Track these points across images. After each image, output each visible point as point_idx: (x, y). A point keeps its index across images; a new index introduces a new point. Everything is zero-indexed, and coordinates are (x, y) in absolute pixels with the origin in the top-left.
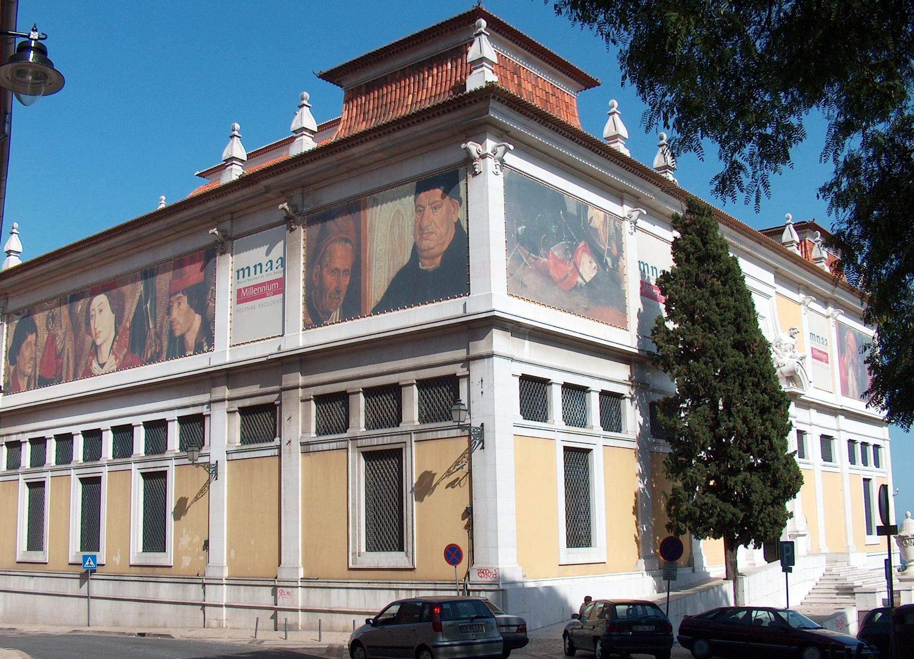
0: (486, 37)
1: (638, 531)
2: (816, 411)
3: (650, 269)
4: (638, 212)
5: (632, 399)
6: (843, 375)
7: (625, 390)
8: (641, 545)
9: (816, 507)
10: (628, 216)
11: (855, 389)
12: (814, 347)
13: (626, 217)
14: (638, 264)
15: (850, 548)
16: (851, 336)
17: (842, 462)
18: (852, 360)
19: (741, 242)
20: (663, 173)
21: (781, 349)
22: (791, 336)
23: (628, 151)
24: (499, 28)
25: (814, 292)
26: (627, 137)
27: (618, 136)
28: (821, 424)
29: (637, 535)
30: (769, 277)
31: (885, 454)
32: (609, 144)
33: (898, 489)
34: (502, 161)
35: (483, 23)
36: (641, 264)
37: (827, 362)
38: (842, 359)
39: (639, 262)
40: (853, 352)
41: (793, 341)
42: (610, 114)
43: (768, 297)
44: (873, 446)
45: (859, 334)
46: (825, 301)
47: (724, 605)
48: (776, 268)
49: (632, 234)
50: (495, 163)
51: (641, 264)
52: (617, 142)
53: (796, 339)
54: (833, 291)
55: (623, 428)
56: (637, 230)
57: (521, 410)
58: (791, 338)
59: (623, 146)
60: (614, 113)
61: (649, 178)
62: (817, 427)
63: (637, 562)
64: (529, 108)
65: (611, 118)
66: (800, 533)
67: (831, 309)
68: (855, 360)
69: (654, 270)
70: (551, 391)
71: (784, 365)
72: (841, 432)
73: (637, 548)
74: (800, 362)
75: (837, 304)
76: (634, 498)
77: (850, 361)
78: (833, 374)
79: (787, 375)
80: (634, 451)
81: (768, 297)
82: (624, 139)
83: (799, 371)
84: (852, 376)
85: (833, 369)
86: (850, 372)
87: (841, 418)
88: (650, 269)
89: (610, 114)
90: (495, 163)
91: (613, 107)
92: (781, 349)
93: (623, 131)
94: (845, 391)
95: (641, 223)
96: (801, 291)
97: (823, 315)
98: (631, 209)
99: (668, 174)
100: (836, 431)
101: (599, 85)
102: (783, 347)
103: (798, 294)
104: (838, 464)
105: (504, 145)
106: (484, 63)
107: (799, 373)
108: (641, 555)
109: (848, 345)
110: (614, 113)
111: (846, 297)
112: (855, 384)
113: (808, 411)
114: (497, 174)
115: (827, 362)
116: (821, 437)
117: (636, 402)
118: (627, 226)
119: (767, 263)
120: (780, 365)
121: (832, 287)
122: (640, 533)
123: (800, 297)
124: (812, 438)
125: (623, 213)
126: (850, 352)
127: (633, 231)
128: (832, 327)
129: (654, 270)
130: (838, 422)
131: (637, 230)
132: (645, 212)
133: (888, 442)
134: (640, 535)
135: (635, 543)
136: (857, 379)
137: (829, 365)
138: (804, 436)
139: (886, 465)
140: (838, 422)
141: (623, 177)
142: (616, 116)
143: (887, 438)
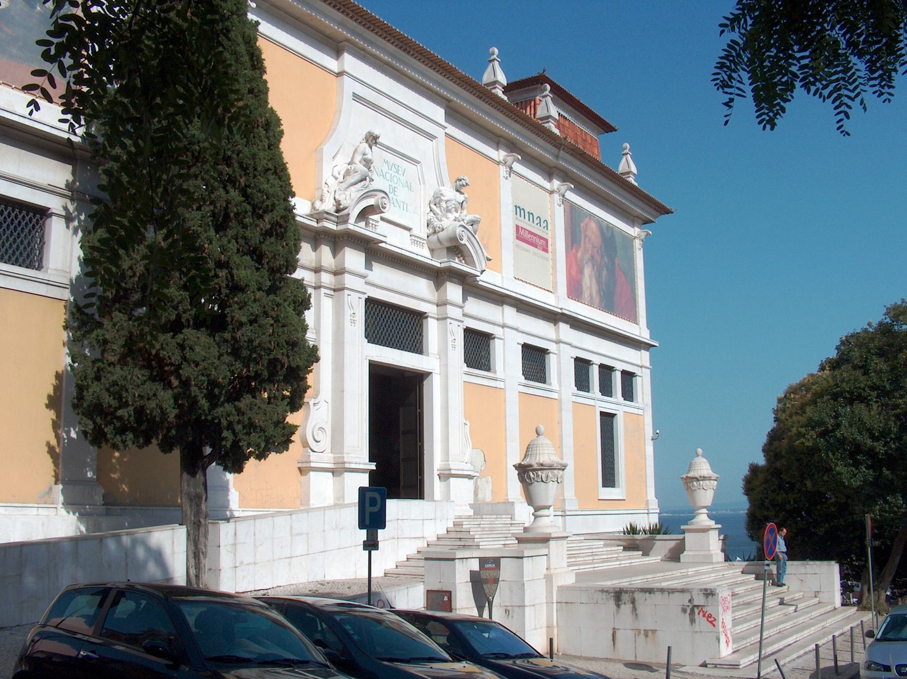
0: (498, 63)
1: (57, 437)
2: (515, 309)
3: (527, 215)
4: (566, 186)
5: (68, 219)
6: (574, 273)
7: (55, 204)
8: (60, 461)
9: (506, 441)
10: (557, 189)
11: (594, 295)
12: (521, 224)
13: (502, 161)
14: (515, 208)
15: (567, 502)
16: (593, 225)
17: (560, 386)
18: (593, 257)
19: (371, 43)
20: (546, 123)
21: (440, 207)
22: (457, 191)
23: (558, 131)
24: (561, 95)
25: (524, 152)
26: (636, 173)
27: (549, 117)
28: (574, 343)
29: (54, 442)
30: (439, 113)
31: (643, 386)
32: (544, 123)
33: (658, 431)
34: (511, 168)
35: (548, 87)
36: (518, 209)
37: (545, 250)
38: (574, 251)
39: (516, 206)
40: (594, 247)
41: (461, 198)
42: (624, 155)
43: (431, 137)
44: (622, 372)
45: (608, 227)
46: (549, 172)
47: (152, 573)
48: (449, 101)
49: (506, 179)
50: (505, 170)
51: (518, 209)
52: (548, 122)
53: (466, 195)
54: (557, 157)
55: (491, 367)
56: (512, 175)
57: (465, 359)
58: (458, 193)
59: (553, 126)
60: (627, 154)
61: (521, 121)
62: (515, 332)
63: (51, 489)
64: (424, 54)
65: (491, 65)
66: (453, 472)
67: (556, 183)
68: (598, 258)
69: (531, 216)
70: (51, 225)
71: (443, 230)
72: (561, 344)
73: (52, 466)
74: (470, 228)
75: (566, 177)
76: (54, 381)
77: (587, 256)
78: (554, 267)
79: (448, 245)
80: (63, 303)
81: (431, 137)
82: (634, 174)
83: (465, 238)
84: (590, 276)
85: (554, 260)
86: (588, 271)
87: (564, 327)
88: (527, 215)
89: (624, 155)
90: (505, 170)
91: (626, 149)
92: (440, 207)
93: (634, 169)
94: (575, 292)
95: (517, 167)
96: (500, 146)
97: (330, 71)
98: (506, 154)
99: (550, 124)
100: (640, 368)
101: (616, 130)
102: (443, 204)
103: (498, 150)
104: (499, 374)
105: (514, 155)
106: (497, 85)
107: (464, 241)
108: (60, 477)
109: (586, 237)
110: (627, 154)
111: (580, 169)
112: (595, 288)
113: (639, 352)
114: (560, 206)
115: (545, 250)
116: (575, 359)
117: (76, 223)
118: (503, 170)
119: (429, 89)
120: (437, 229)
121: (554, 150)
122: (62, 442)
123: (500, 155)
124: (504, 344)
125: (635, 234)
126: (589, 246)
127: (508, 175)
128: (637, 250)
129: (531, 216)
130: (557, 331)
131: (512, 175)
132: (573, 186)
133: (649, 370)
134: (61, 445)
135: (48, 457)
136: (599, 283)
137: (549, 255)
138: (634, 379)
139: (643, 400)
140: (557, 331)
141: (617, 193)
142: (629, 156)
143: (648, 365)
